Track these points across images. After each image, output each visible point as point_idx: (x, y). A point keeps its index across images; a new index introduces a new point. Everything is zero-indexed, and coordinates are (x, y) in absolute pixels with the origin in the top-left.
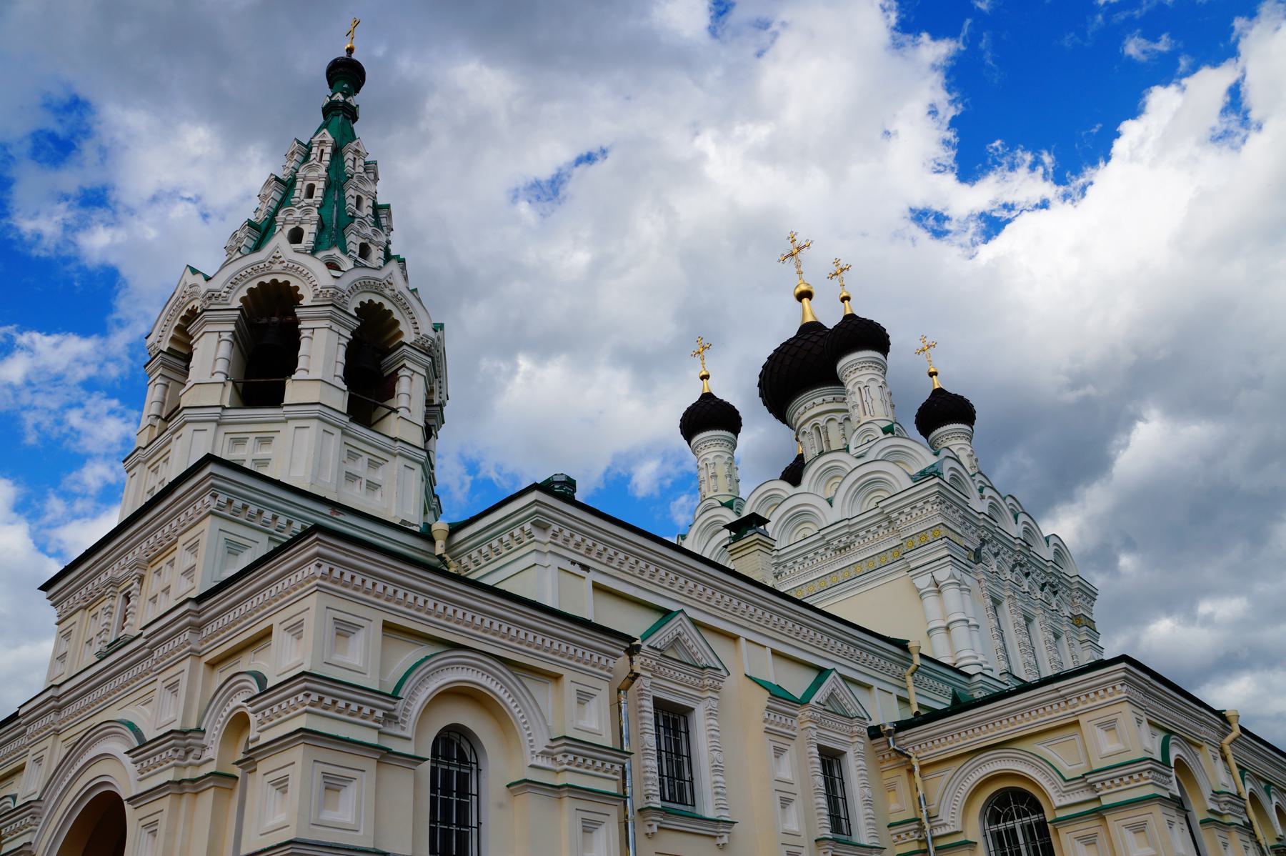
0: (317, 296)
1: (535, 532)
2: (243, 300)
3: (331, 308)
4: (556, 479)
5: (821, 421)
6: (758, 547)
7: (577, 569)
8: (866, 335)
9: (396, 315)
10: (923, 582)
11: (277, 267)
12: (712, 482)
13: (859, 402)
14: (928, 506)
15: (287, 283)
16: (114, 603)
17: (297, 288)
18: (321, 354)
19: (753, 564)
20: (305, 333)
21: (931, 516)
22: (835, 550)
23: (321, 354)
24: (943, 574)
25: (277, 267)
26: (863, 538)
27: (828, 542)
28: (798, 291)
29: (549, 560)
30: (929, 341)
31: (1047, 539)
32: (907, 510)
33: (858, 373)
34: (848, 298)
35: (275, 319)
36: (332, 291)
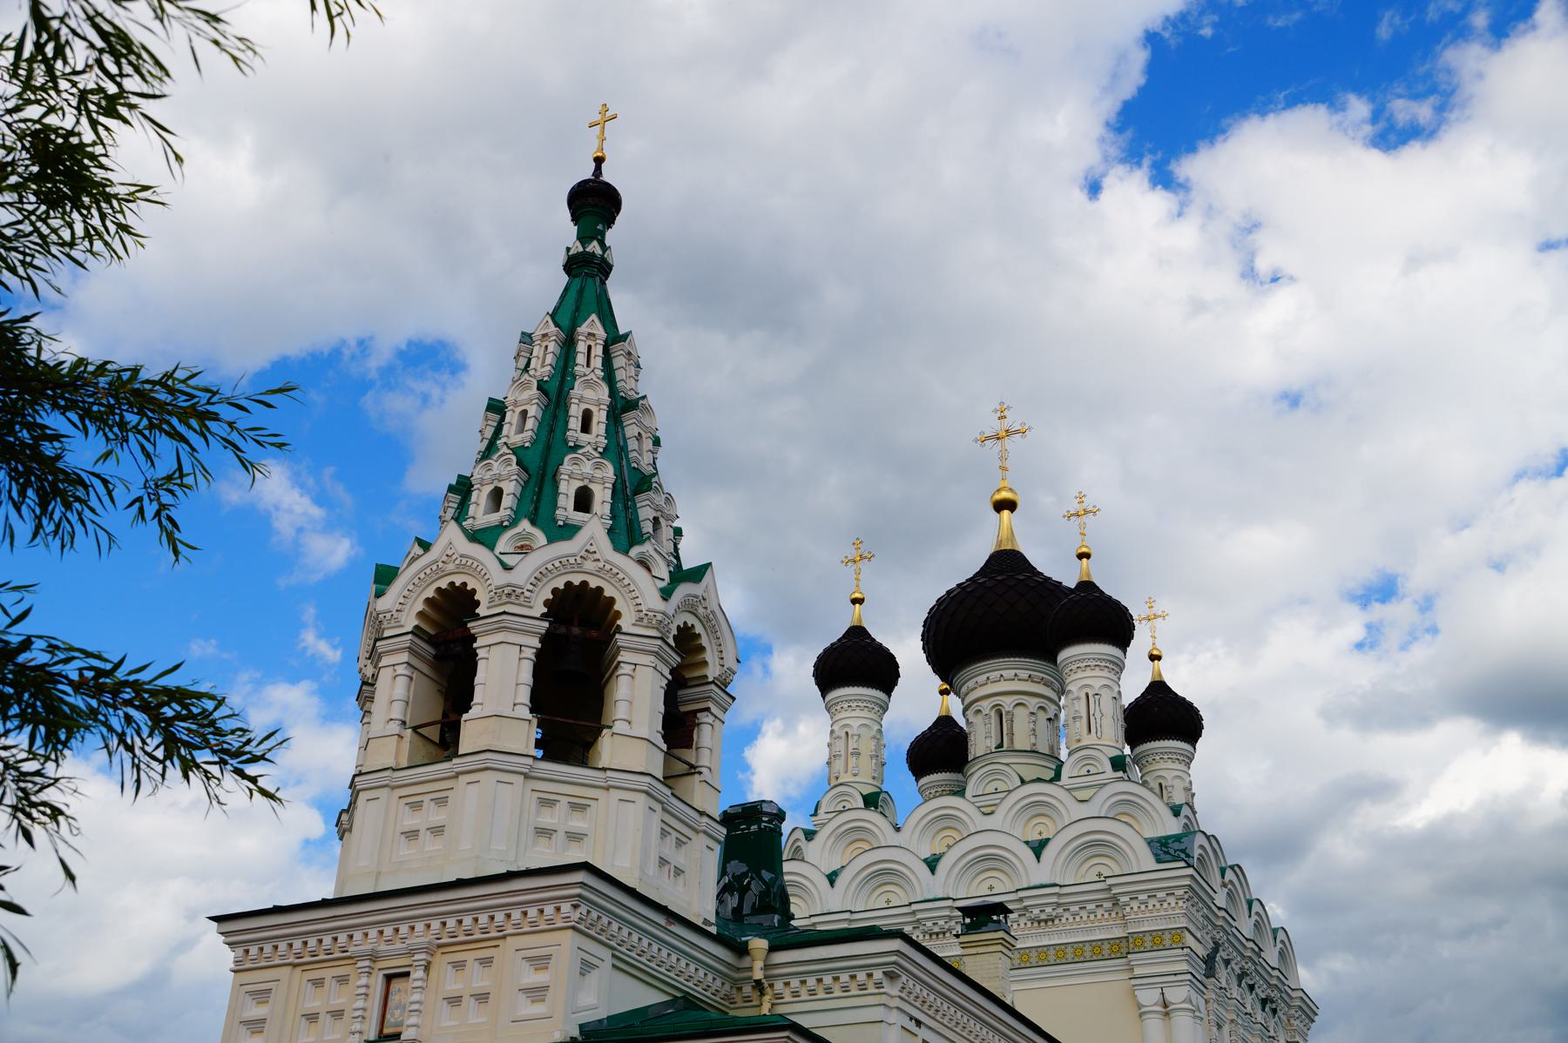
0: (641, 619)
1: (886, 983)
2: (546, 603)
3: (659, 642)
4: (766, 808)
5: (1007, 703)
6: (1000, 948)
7: (912, 1026)
8: (1107, 621)
9: (704, 641)
10: (1149, 997)
11: (589, 565)
12: (852, 761)
13: (1084, 714)
14: (1172, 900)
15: (600, 590)
16: (372, 981)
17: (474, 591)
18: (505, 672)
19: (986, 966)
20: (481, 653)
21: (1171, 914)
22: (1032, 921)
23: (505, 672)
24: (1177, 995)
25: (451, 567)
26: (1074, 915)
27: (1025, 908)
28: (998, 497)
29: (894, 1017)
30: (1013, 421)
31: (1275, 931)
32: (1143, 897)
33: (1089, 673)
34: (1087, 556)
35: (576, 630)
36: (659, 616)
